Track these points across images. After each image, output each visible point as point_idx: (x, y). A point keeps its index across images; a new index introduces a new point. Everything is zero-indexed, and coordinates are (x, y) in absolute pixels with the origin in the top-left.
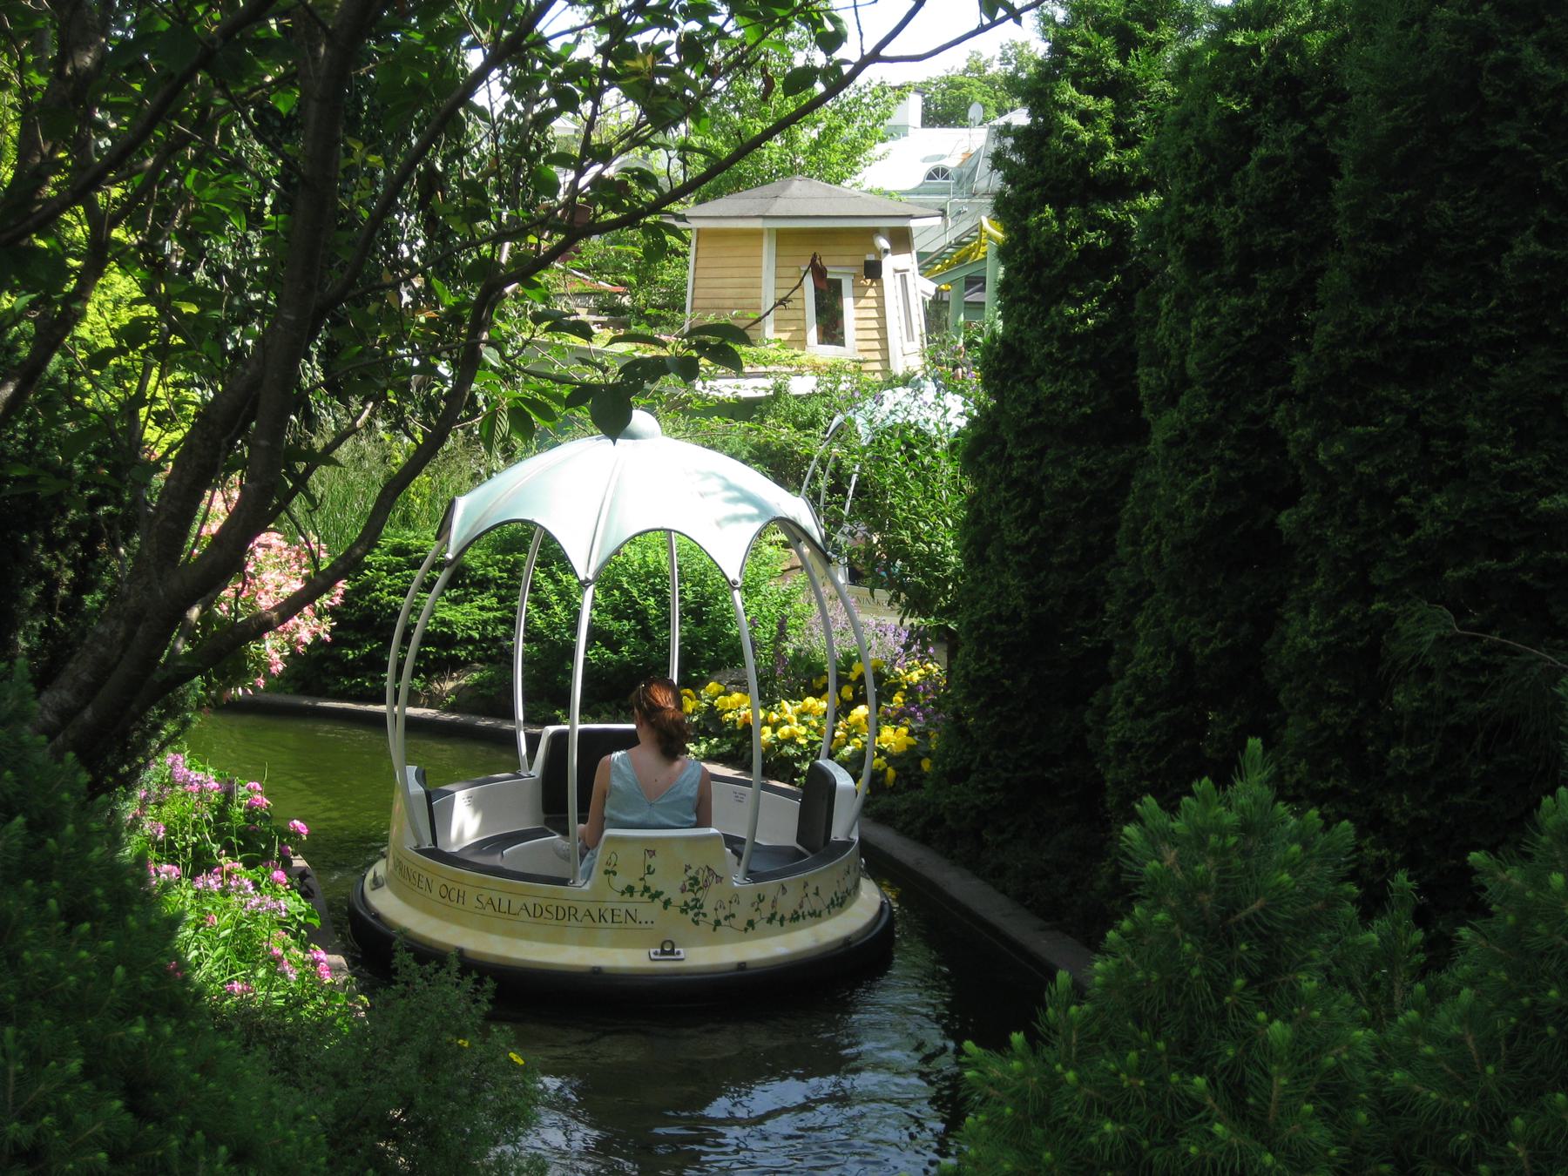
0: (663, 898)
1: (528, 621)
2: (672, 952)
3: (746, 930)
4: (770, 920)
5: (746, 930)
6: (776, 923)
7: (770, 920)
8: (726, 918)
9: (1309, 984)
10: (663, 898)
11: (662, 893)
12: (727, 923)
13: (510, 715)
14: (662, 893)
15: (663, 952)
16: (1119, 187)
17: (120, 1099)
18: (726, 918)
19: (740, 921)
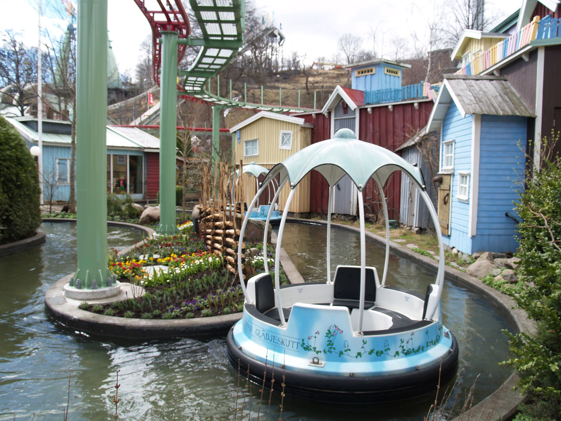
2: (318, 363)
3: (357, 357)
5: (357, 357)
8: (346, 351)
15: (314, 363)
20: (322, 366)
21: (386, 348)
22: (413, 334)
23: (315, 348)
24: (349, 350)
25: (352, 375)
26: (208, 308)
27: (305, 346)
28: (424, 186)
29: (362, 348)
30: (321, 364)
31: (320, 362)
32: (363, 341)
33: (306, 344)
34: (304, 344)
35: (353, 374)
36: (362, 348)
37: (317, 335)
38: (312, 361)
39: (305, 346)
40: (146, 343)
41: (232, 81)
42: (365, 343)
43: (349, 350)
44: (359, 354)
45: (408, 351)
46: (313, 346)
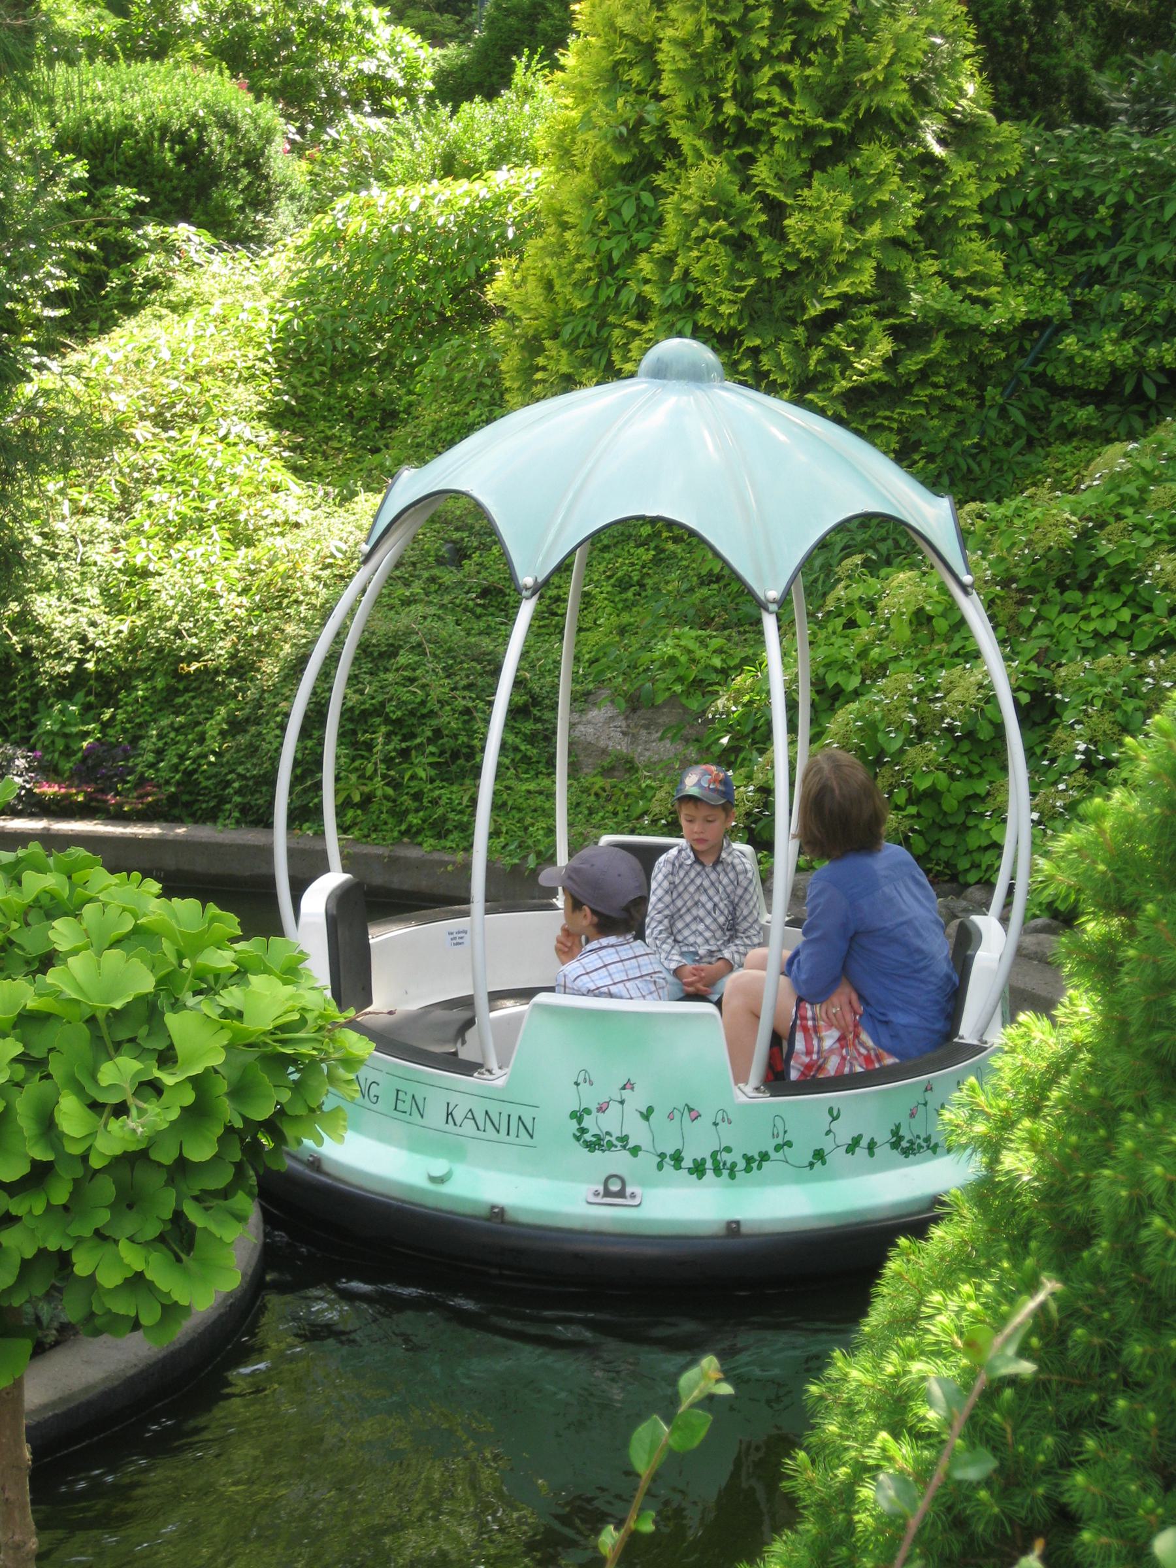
0: (864, 1143)
1: (665, 849)
2: (621, 1194)
3: (811, 1165)
4: (852, 1148)
5: (811, 1165)
6: (861, 1152)
7: (852, 1148)
8: (778, 1148)
9: (16, 287)
10: (864, 1143)
11: (860, 1136)
12: (779, 1155)
13: (266, 822)
14: (860, 1136)
15: (608, 1193)
16: (698, 96)
17: (807, 1391)
18: (778, 1148)
19: (802, 1152)
20: (636, 1202)
21: (780, 1141)
22: (929, 1088)
23: (624, 1139)
24: (789, 1144)
25: (497, 1214)
26: (907, 31)
27: (588, 1137)
28: (967, 579)
29: (828, 1132)
30: (633, 1196)
31: (629, 1190)
32: (831, 1110)
33: (594, 1130)
34: (583, 1131)
35: (738, 1223)
36: (828, 1132)
37: (626, 1094)
38: (601, 1189)
39: (588, 1137)
40: (469, 1305)
41: (64, 318)
42: (834, 1119)
43: (789, 1144)
44: (819, 1155)
45: (911, 1142)
46: (616, 1133)
